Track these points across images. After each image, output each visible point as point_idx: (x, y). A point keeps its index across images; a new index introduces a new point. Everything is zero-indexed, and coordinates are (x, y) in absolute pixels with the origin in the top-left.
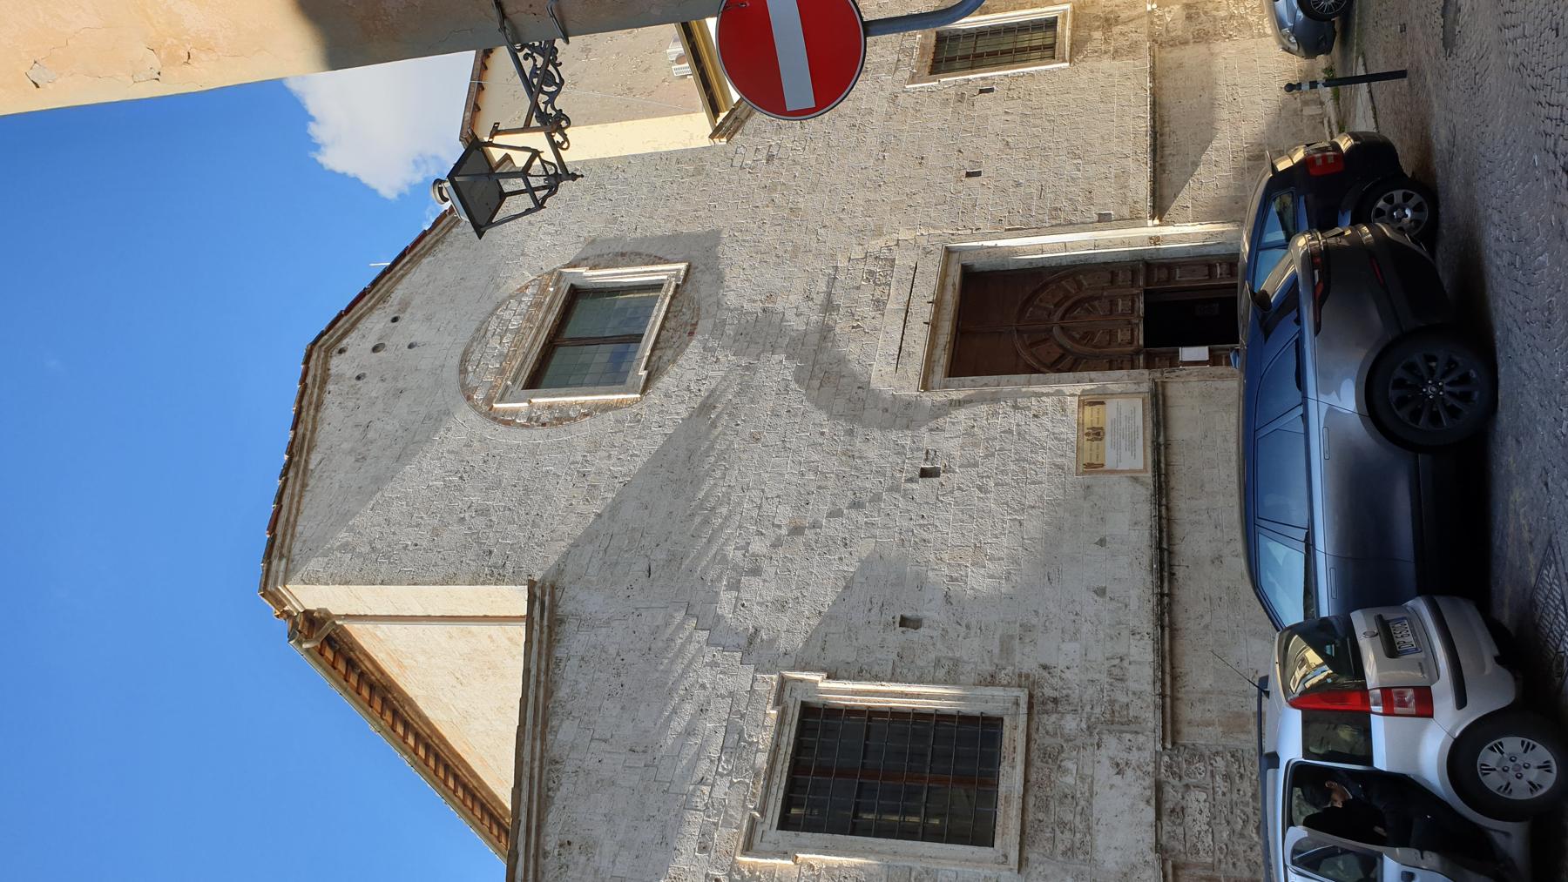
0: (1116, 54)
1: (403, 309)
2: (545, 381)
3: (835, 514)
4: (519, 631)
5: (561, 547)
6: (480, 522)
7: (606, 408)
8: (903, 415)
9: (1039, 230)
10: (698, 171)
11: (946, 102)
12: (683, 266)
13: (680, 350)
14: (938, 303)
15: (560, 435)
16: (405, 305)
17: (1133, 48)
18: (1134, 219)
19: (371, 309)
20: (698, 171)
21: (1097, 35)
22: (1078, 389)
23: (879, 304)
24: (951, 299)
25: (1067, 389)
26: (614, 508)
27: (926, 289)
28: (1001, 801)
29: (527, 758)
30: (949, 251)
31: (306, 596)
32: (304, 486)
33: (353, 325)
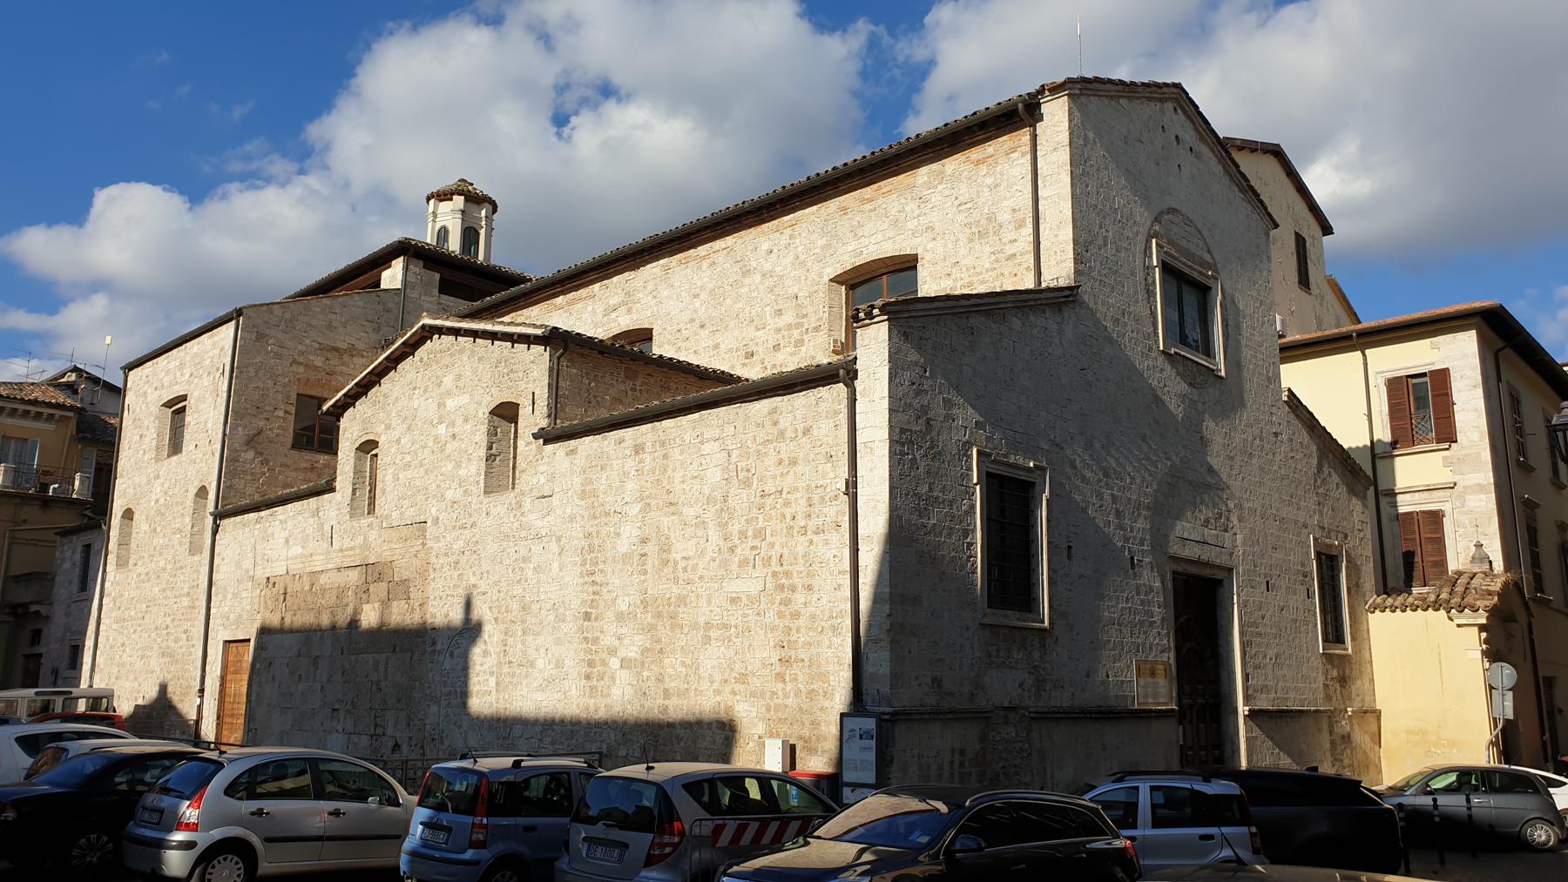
0: (1326, 686)
1: (1197, 157)
2: (570, 371)
3: (1114, 499)
4: (1029, 284)
5: (1091, 305)
6: (1100, 242)
7: (1156, 328)
8: (1159, 539)
9: (1242, 633)
10: (1269, 379)
11: (1303, 565)
12: (1223, 373)
13: (1183, 377)
14: (1207, 564)
15: (1141, 295)
16: (1198, 156)
17: (1328, 698)
18: (1248, 699)
19: (1196, 130)
20: (1269, 379)
21: (1335, 673)
22: (1172, 661)
23: (1206, 523)
24: (1208, 573)
25: (1172, 654)
26: (1109, 339)
27: (1207, 554)
28: (116, 521)
29: (972, 302)
30: (1230, 570)
31: (1056, 113)
32: (1111, 97)
33: (1188, 117)
